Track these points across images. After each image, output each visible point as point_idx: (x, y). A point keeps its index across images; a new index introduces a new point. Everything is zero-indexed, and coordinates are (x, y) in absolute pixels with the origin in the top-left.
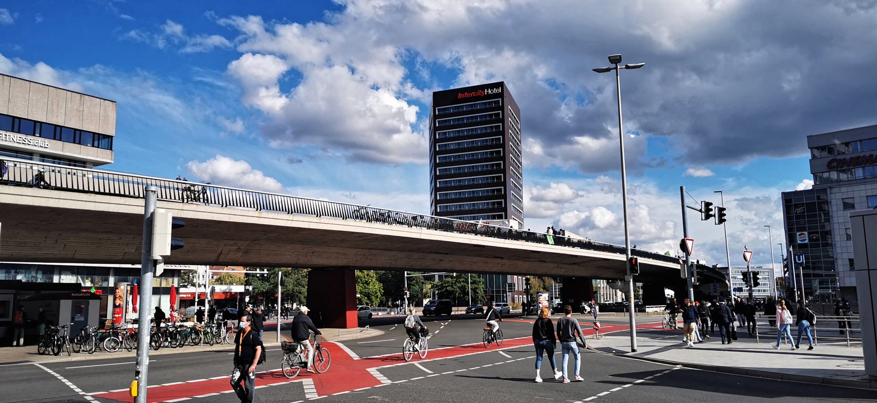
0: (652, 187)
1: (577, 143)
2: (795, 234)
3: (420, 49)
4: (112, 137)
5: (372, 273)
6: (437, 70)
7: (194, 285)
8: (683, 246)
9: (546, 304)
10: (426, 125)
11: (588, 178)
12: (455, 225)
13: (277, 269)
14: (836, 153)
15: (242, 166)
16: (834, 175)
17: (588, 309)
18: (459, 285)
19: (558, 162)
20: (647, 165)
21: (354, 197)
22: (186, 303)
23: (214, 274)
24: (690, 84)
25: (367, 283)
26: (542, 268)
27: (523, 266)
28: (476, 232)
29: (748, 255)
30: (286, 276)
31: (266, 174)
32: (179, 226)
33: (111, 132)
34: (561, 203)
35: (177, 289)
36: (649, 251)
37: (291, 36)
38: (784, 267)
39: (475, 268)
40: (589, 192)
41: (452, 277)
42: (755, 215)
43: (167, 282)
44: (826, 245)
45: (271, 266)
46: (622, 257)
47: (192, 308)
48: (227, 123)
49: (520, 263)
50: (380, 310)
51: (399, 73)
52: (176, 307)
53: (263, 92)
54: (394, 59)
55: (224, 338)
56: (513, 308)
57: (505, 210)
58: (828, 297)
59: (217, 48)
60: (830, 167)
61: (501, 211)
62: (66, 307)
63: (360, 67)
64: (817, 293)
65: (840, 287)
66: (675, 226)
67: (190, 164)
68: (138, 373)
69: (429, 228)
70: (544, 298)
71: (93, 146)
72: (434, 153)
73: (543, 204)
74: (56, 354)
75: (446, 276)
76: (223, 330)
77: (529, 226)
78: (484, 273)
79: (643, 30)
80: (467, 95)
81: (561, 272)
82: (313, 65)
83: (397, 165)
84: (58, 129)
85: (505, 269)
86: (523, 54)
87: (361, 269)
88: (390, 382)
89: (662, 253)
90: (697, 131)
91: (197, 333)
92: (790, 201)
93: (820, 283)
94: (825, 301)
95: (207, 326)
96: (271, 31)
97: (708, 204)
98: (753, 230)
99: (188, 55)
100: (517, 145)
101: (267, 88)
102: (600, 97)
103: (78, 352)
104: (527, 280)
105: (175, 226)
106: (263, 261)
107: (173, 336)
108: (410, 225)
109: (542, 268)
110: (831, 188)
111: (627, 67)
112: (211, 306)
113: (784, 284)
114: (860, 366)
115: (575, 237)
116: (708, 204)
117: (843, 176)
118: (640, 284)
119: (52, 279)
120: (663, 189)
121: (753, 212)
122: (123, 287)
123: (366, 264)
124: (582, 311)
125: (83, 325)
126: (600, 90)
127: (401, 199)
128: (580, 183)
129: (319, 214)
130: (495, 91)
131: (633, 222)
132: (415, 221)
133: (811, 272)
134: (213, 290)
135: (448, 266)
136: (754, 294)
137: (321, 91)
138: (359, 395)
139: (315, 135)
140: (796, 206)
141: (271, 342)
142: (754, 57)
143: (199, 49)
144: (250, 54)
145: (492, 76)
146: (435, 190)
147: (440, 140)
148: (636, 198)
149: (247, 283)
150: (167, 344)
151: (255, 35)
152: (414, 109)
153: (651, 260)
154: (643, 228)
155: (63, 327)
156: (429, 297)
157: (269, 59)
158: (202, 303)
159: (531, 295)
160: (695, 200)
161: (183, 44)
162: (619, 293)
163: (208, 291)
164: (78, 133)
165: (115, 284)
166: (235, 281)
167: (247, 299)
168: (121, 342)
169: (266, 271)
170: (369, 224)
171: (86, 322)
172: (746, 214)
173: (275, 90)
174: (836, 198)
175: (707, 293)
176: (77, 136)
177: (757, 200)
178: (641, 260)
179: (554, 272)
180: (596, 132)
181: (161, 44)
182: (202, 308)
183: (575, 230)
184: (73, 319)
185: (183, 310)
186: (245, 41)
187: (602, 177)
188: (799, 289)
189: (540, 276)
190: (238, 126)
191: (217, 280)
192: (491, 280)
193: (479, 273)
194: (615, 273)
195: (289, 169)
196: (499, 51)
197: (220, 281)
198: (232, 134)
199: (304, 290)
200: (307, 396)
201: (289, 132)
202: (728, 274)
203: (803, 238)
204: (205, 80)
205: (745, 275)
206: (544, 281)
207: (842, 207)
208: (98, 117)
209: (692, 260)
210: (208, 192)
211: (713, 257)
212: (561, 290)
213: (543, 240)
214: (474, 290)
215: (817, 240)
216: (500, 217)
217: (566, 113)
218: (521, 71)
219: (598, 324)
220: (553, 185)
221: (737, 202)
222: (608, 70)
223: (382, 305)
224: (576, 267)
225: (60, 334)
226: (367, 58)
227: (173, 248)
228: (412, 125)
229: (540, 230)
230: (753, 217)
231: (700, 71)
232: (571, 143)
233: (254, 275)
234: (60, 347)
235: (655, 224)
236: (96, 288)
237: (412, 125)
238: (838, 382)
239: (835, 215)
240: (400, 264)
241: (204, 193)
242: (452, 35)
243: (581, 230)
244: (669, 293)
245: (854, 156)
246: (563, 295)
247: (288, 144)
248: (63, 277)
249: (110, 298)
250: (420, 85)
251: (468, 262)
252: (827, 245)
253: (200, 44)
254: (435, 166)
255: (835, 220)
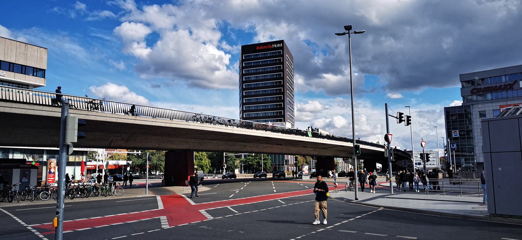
0: (368, 104)
1: (324, 78)
2: (452, 132)
3: (230, 21)
4: (45, 70)
5: (204, 153)
6: (240, 33)
7: (96, 160)
8: (386, 138)
9: (307, 172)
10: (237, 65)
11: (329, 98)
12: (254, 126)
13: (147, 151)
14: (476, 85)
15: (124, 89)
16: (475, 98)
17: (332, 175)
18: (256, 161)
19: (313, 89)
20: (363, 91)
21: (192, 109)
22: (91, 171)
23: (108, 154)
24: (389, 44)
25: (201, 159)
26: (305, 151)
27: (294, 149)
28: (266, 130)
29: (423, 144)
30: (152, 155)
31: (138, 94)
32: (83, 125)
33: (44, 67)
34: (317, 112)
35: (85, 163)
36: (368, 141)
37: (152, 12)
38: (445, 151)
39: (265, 151)
40: (331, 106)
41: (252, 156)
42: (427, 121)
43: (79, 159)
44: (469, 138)
45: (143, 149)
46: (350, 145)
47: (95, 174)
48: (115, 63)
49: (292, 148)
50: (209, 176)
51: (218, 35)
52: (85, 173)
53: (135, 45)
54: (215, 27)
55: (114, 192)
56: (288, 175)
57: (284, 116)
58: (470, 168)
59: (107, 18)
60: (472, 93)
61: (281, 117)
62: (16, 174)
63: (195, 31)
64: (464, 166)
65: (477, 163)
66: (382, 126)
67: (91, 88)
68: (58, 213)
69: (238, 127)
70: (306, 168)
71: (33, 75)
72: (242, 82)
73: (304, 113)
74: (10, 202)
75: (248, 156)
76: (113, 187)
77: (299, 126)
78: (271, 154)
79: (361, 12)
80: (262, 48)
81: (316, 153)
82: (165, 29)
83: (218, 90)
84: (12, 65)
85: (283, 151)
86: (292, 25)
87: (198, 151)
88: (212, 218)
89: (375, 142)
90: (393, 71)
91: (97, 189)
92: (449, 112)
93: (465, 160)
94: (468, 171)
95: (103, 185)
96: (140, 8)
97: (401, 114)
98: (426, 129)
99: (89, 22)
100: (291, 78)
101: (138, 43)
102: (336, 51)
103: (24, 200)
104: (296, 158)
105: (79, 125)
106: (137, 146)
107: (82, 191)
108: (226, 125)
109: (305, 151)
110: (472, 105)
111: (355, 33)
112: (106, 173)
113: (445, 161)
114: (485, 208)
115: (324, 133)
116: (401, 114)
117: (480, 98)
118: (362, 161)
119: (8, 156)
120: (375, 104)
121: (426, 119)
122: (54, 161)
123: (201, 148)
124: (328, 176)
125: (27, 184)
126: (337, 47)
127: (222, 109)
128: (325, 101)
129: (171, 118)
130: (279, 45)
131: (357, 124)
132: (230, 123)
133: (460, 153)
134: (108, 163)
135: (250, 150)
136: (427, 166)
137: (171, 45)
138: (194, 225)
139: (169, 71)
140: (452, 115)
141: (142, 194)
142: (421, 31)
143: (96, 18)
144: (127, 23)
145: (271, 37)
146: (242, 104)
147: (245, 75)
148: (359, 110)
149: (129, 159)
150: (78, 195)
151: (130, 12)
152: (228, 56)
153: (368, 146)
154: (363, 128)
155: (15, 185)
156: (238, 168)
157: (139, 25)
158: (100, 171)
159: (299, 167)
160: (394, 111)
161: (86, 16)
162: (350, 166)
163: (104, 164)
164: (24, 67)
165: (47, 159)
166: (121, 158)
167: (128, 169)
168: (50, 195)
169: (140, 152)
170: (202, 125)
171: (29, 182)
172: (422, 120)
173: (143, 44)
174: (475, 111)
175: (400, 166)
176: (23, 69)
177: (428, 112)
178: (362, 146)
179: (312, 153)
180: (336, 72)
181: (73, 15)
182: (101, 174)
183: (324, 128)
184: (21, 181)
185: (89, 175)
186: (124, 15)
187: (338, 98)
188: (453, 163)
189: (304, 156)
190: (122, 66)
191: (110, 158)
192: (275, 158)
193: (268, 154)
194: (348, 154)
195: (151, 91)
196: (278, 23)
197: (112, 158)
198: (118, 70)
199: (163, 164)
200: (163, 227)
201: (152, 69)
202: (412, 155)
203: (456, 134)
204: (98, 35)
205: (421, 155)
206: (306, 159)
207: (479, 116)
208: (36, 58)
209: (392, 146)
210: (104, 104)
211: (403, 144)
212: (316, 164)
213: (305, 134)
214: (265, 164)
215: (464, 135)
216: (281, 121)
217: (318, 61)
218: (291, 34)
219: (337, 184)
220: (310, 102)
221: (417, 113)
222: (344, 34)
223: (210, 172)
224: (325, 150)
225: (13, 190)
226: (199, 25)
227: (79, 137)
228: (226, 65)
229: (303, 128)
230: (426, 122)
231: (395, 36)
232: (320, 77)
233: (133, 155)
234: (12, 198)
235: (371, 126)
236: (36, 162)
237: (226, 65)
238: (472, 217)
239: (474, 120)
240: (221, 148)
241: (101, 104)
242: (249, 13)
243: (327, 129)
244: (379, 166)
245: (486, 86)
246: (317, 167)
247: (152, 76)
248: (15, 155)
249: (44, 168)
250: (231, 43)
251: (261, 147)
252: (469, 138)
253: (97, 16)
254: (242, 90)
255: (475, 124)
